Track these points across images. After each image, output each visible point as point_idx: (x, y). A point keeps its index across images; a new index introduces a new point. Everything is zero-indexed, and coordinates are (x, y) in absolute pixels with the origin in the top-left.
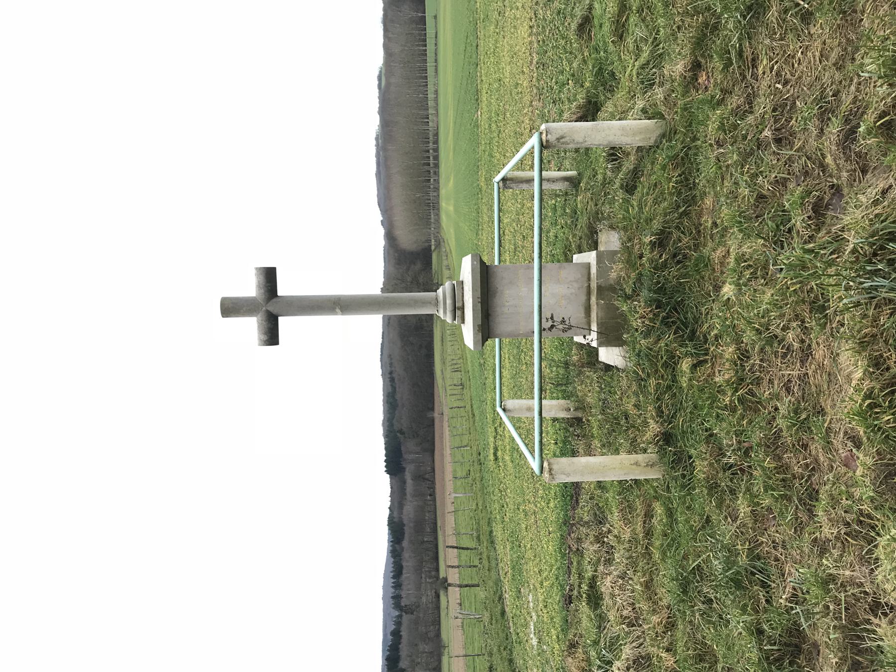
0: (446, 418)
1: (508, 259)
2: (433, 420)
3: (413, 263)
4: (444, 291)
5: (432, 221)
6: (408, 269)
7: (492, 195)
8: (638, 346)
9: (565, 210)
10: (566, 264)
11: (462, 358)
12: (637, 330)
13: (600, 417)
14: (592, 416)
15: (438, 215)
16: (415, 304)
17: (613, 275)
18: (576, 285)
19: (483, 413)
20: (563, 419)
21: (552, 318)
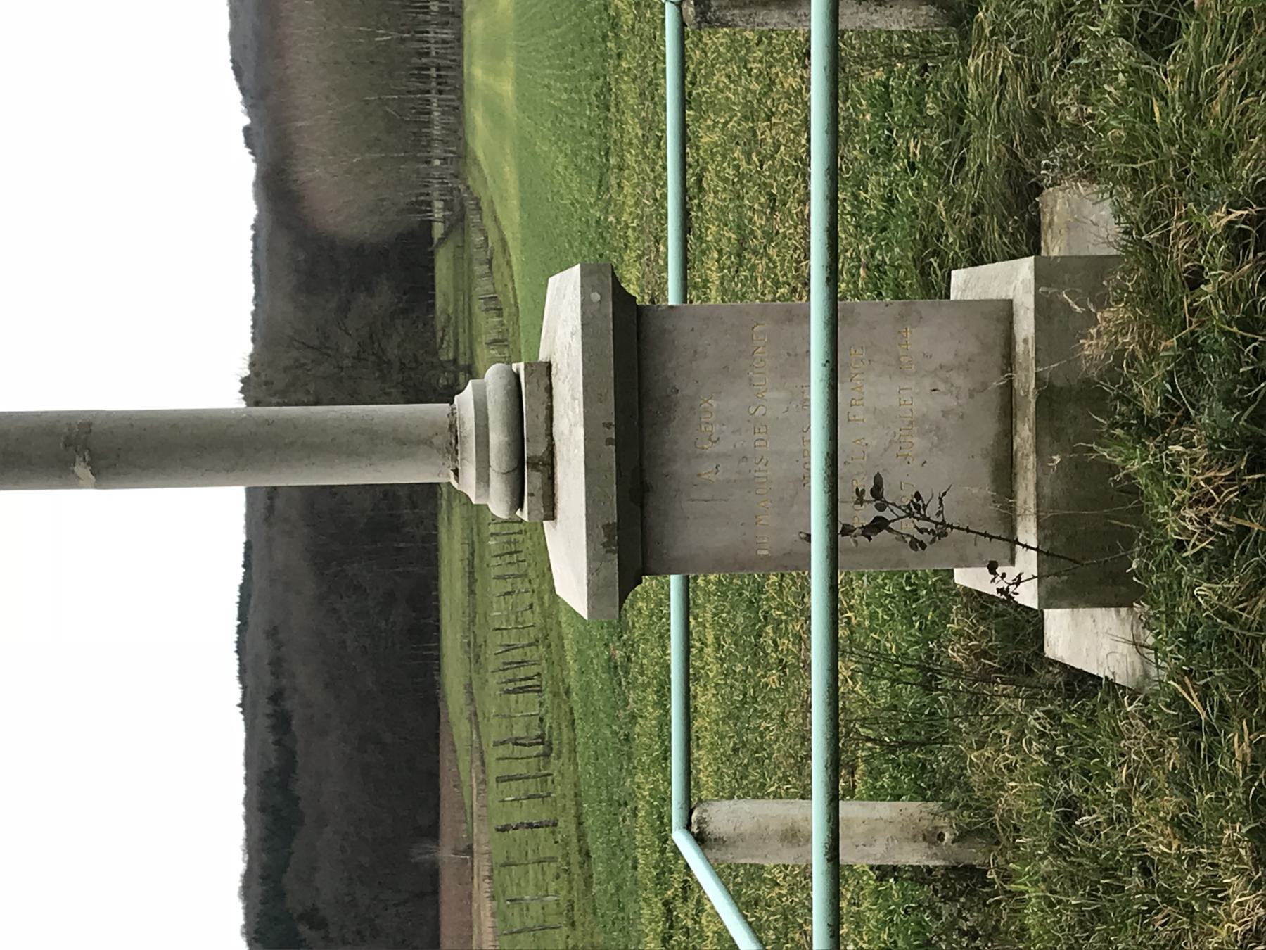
0: (481, 866)
1: (715, 277)
2: (433, 875)
3: (358, 289)
4: (480, 397)
5: (436, 131)
6: (344, 309)
7: (655, 41)
8: (1184, 605)
9: (920, 105)
10: (922, 305)
11: (543, 639)
12: (1180, 546)
13: (1044, 866)
14: (1023, 859)
15: (456, 111)
16: (368, 448)
17: (1092, 348)
18: (960, 381)
19: (620, 848)
20: (916, 869)
21: (877, 491)
